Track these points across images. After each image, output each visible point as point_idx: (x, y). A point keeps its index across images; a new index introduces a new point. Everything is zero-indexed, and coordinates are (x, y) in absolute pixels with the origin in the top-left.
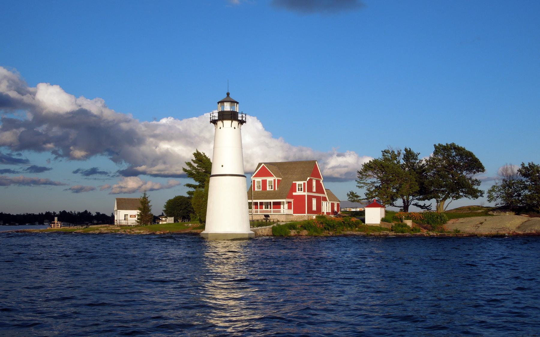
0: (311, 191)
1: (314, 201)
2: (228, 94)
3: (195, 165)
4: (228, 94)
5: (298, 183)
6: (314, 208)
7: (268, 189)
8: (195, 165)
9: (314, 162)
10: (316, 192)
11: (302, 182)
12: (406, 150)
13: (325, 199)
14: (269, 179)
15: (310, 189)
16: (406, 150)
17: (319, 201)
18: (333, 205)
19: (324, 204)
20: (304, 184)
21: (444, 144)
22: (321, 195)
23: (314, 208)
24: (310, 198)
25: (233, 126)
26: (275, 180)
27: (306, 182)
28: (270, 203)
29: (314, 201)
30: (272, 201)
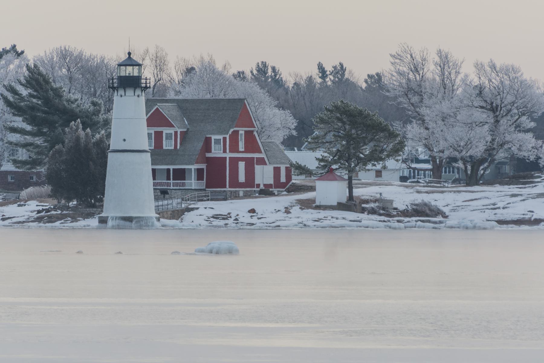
0: (238, 152)
1: (242, 165)
2: (129, 54)
3: (24, 92)
4: (129, 54)
5: (214, 137)
6: (242, 178)
7: (164, 148)
8: (24, 92)
9: (241, 101)
10: (246, 151)
11: (221, 137)
12: (439, 52)
13: (261, 162)
14: (166, 131)
15: (234, 148)
16: (439, 52)
17: (250, 164)
18: (277, 171)
19: (258, 168)
20: (225, 139)
21: (303, 165)
22: (256, 155)
23: (242, 178)
24: (234, 162)
25: (136, 94)
26: (176, 133)
27: (228, 137)
28: (168, 170)
29: (242, 165)
30: (171, 167)
